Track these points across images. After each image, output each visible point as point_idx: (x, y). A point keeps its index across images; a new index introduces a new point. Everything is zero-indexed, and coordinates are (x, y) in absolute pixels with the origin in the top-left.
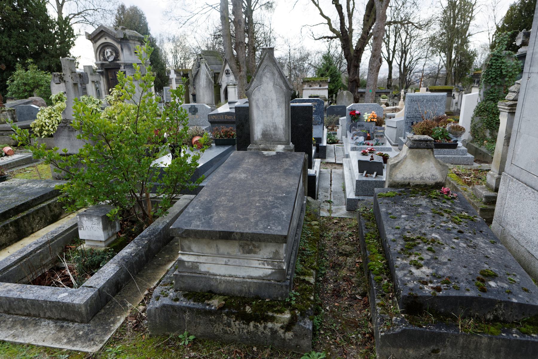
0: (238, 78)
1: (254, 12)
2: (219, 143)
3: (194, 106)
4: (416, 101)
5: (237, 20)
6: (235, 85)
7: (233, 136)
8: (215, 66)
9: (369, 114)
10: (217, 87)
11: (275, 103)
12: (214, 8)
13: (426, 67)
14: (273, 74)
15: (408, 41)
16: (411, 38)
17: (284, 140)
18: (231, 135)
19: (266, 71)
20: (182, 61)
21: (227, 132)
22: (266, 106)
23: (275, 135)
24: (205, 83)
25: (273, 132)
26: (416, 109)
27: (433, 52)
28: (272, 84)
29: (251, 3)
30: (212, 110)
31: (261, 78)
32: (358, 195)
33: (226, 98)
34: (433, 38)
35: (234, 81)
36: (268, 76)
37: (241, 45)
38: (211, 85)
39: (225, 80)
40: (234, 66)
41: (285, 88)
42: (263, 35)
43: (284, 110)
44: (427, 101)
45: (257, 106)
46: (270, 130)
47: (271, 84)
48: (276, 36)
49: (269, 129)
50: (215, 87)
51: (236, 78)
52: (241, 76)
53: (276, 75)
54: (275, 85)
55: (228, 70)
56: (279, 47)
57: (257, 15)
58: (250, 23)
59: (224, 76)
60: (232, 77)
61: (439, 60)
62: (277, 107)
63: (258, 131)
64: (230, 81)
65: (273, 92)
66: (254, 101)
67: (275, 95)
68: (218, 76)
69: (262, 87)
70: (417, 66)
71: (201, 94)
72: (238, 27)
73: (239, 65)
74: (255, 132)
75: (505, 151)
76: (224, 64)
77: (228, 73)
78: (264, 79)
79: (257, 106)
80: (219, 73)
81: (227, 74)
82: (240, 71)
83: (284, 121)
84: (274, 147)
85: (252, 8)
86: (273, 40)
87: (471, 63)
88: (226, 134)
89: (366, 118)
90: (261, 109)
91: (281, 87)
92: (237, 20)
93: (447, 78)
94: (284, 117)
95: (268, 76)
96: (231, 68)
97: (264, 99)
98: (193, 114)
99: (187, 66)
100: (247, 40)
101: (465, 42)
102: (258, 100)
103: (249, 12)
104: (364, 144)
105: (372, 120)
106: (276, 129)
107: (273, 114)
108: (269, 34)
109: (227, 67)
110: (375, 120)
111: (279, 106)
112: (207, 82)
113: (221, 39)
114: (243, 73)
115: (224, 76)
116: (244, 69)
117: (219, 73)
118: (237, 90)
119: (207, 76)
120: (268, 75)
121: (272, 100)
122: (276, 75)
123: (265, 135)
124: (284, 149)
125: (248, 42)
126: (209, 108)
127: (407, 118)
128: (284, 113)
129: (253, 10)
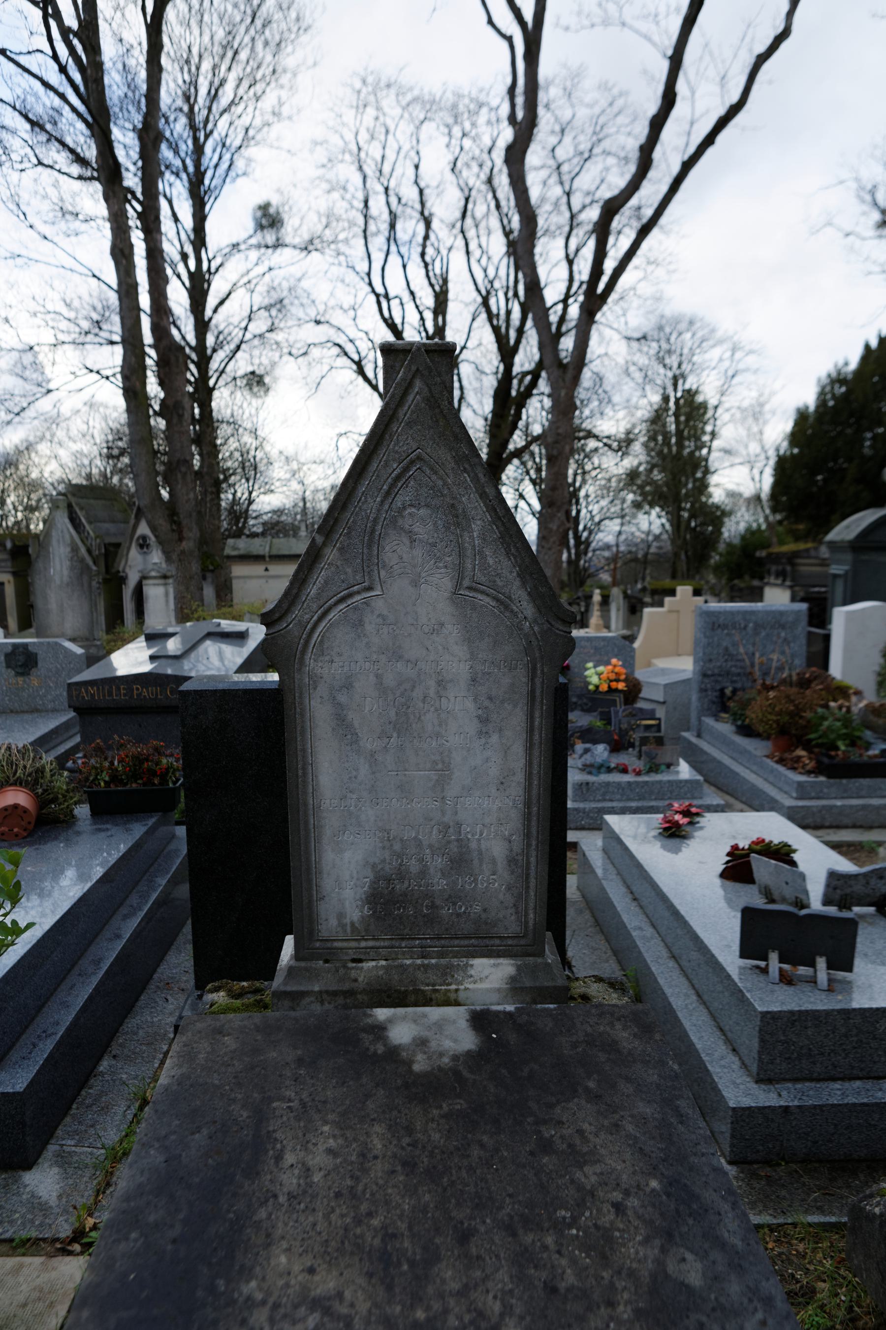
0: (175, 557)
1: (216, 394)
2: (110, 807)
3: (25, 646)
4: (724, 627)
5: (170, 402)
6: (165, 577)
7: (164, 775)
8: (107, 525)
9: (601, 669)
10: (114, 581)
11: (461, 706)
12: (107, 378)
13: (623, 537)
14: (457, 519)
15: (579, 478)
16: (584, 473)
17: (511, 925)
18: (154, 773)
19: (403, 497)
20: (20, 515)
21: (139, 760)
22: (402, 723)
23: (453, 898)
24: (66, 572)
25: (439, 883)
26: (726, 649)
27: (637, 505)
28: (447, 584)
29: (207, 372)
30: (91, 660)
31: (373, 540)
32: (769, 1081)
33: (140, 612)
34: (632, 475)
35: (164, 565)
36: (422, 531)
37: (183, 469)
38: (85, 579)
39: (134, 564)
40: (163, 524)
41: (528, 609)
42: (237, 455)
43: (518, 749)
44: (758, 627)
45: (341, 721)
46: (423, 873)
47: (438, 587)
48: (274, 453)
49: (414, 866)
50: (106, 581)
51: (168, 559)
52: (183, 552)
53: (476, 527)
54: (464, 588)
55: (144, 538)
56: (278, 484)
57: (222, 401)
58: (208, 419)
59: (134, 553)
60: (156, 557)
61: (653, 522)
62: (472, 727)
63: (342, 873)
64: (150, 567)
65: (453, 632)
66: (322, 690)
67: (461, 651)
68: (116, 553)
69: (379, 605)
70: (600, 536)
71: (53, 605)
72: (175, 420)
73: (179, 524)
74: (327, 884)
75: (285, 606)
76: (132, 521)
77: (143, 544)
78: (395, 550)
79: (341, 721)
80: (118, 545)
81: (141, 546)
82: (181, 539)
83: (514, 823)
84: (446, 972)
85: (211, 383)
86: (261, 467)
87: (718, 532)
88: (138, 767)
89: (595, 680)
90: (369, 743)
91: (504, 604)
92: (170, 402)
93: (674, 563)
94: (516, 790)
95: (422, 531)
96: (154, 529)
97: (389, 680)
98: (22, 674)
99: (32, 527)
100: (196, 462)
101: (702, 486)
102: (348, 686)
103: (204, 393)
104: (609, 770)
105: (614, 685)
106: (461, 860)
107: (443, 771)
108: (252, 453)
109: (143, 529)
110: (621, 686)
111: (484, 720)
112: (72, 568)
113: (126, 460)
114: (187, 545)
115: (134, 553)
116: (192, 534)
117: (118, 545)
118: (171, 590)
119: (75, 549)
120: (422, 523)
121: (441, 683)
122: (476, 527)
123: (393, 903)
124: (515, 987)
125: (201, 466)
126: (79, 651)
127: (705, 675)
128: (518, 761)
129: (214, 389)
